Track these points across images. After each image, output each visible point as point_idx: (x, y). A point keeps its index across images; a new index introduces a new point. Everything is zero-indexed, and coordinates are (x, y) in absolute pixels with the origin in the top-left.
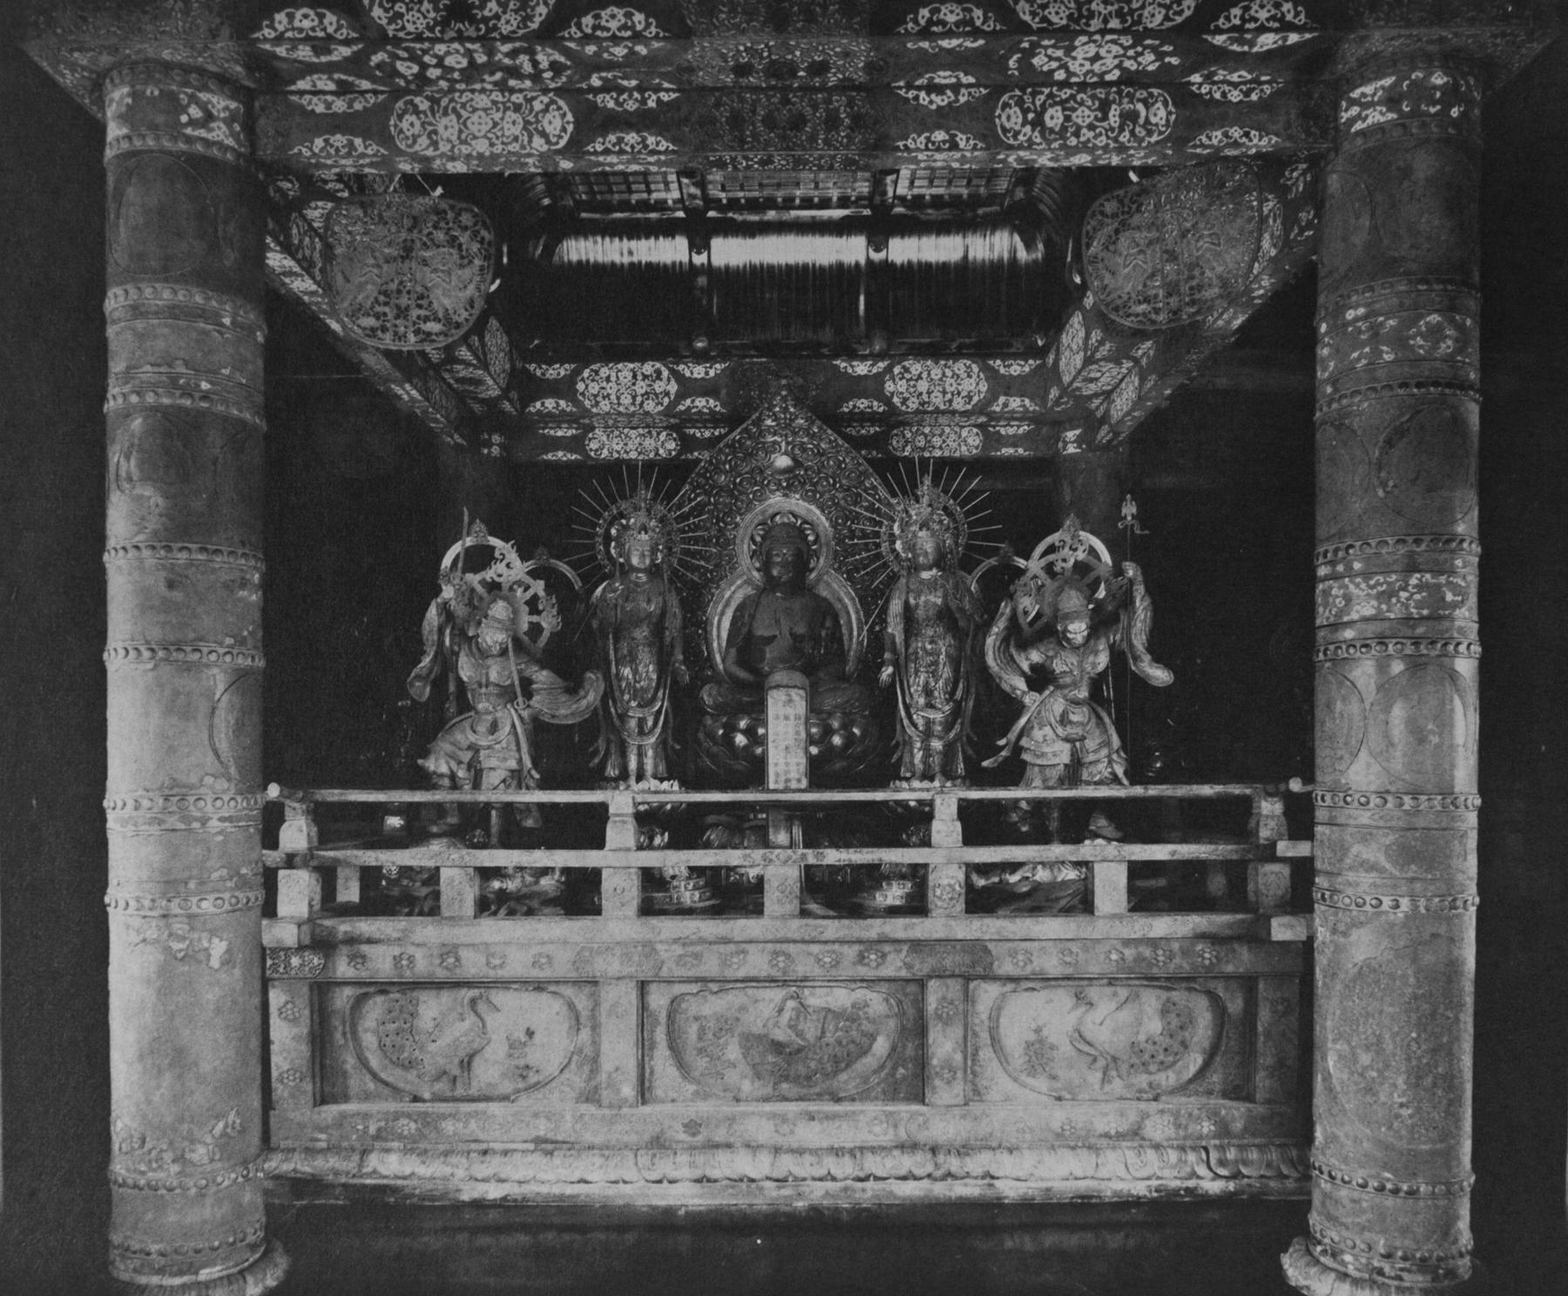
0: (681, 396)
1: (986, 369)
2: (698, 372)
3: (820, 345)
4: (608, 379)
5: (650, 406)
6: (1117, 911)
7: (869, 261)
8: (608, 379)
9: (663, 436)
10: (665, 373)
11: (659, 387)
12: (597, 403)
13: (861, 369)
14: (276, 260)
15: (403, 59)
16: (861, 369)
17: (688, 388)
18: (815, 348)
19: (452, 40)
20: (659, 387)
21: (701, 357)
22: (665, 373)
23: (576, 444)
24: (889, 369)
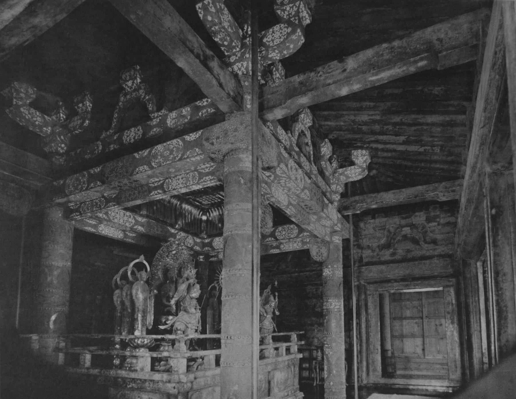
0: (135, 224)
1: (193, 239)
2: (140, 219)
3: (167, 223)
4: (117, 213)
5: (127, 224)
6: (184, 313)
7: (169, 202)
8: (117, 213)
9: (120, 232)
10: (132, 217)
11: (130, 220)
12: (114, 219)
13: (173, 231)
14: (308, 234)
15: (466, 344)
16: (173, 231)
17: (137, 223)
18: (166, 223)
19: (196, 156)
20: (130, 220)
21: (142, 216)
22: (132, 217)
23: (95, 226)
24: (178, 233)
